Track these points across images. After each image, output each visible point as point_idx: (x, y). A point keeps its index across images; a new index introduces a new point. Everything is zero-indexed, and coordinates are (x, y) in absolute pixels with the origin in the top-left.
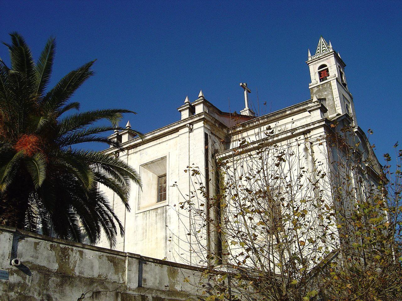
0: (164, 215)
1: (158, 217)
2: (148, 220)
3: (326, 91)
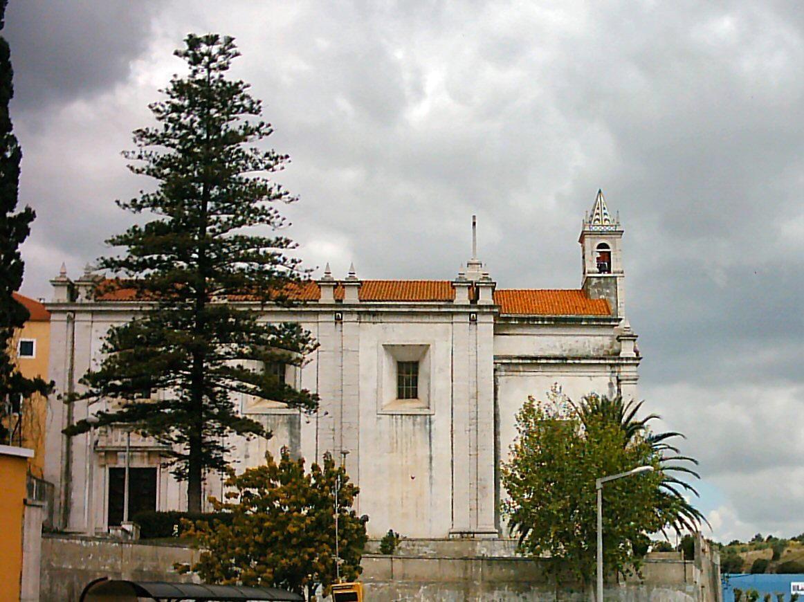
0: (428, 426)
1: (418, 427)
2: (399, 428)
3: (608, 288)
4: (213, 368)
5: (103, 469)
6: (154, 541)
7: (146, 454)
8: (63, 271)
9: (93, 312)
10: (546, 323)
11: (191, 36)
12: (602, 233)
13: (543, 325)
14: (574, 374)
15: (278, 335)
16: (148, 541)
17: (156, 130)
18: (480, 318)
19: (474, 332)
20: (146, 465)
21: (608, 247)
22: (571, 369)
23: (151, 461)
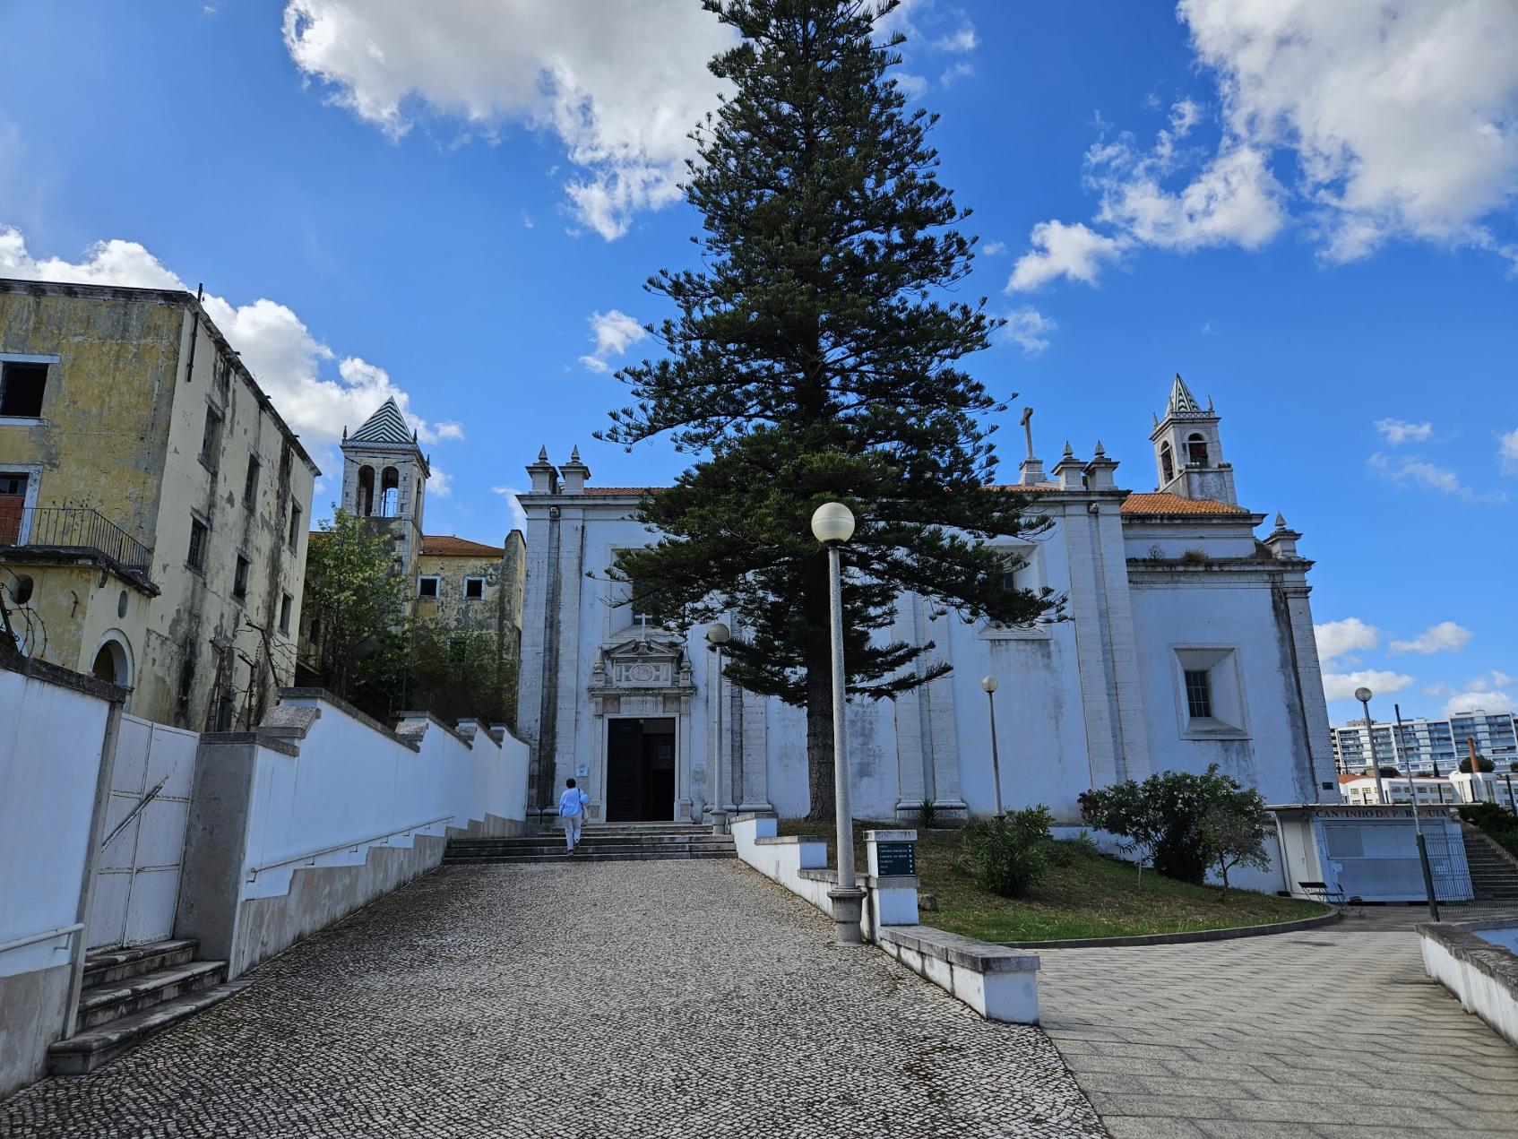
4: (934, 412)
5: (600, 721)
6: (458, 546)
7: (660, 698)
8: (543, 456)
9: (585, 508)
10: (1165, 521)
11: (713, 67)
12: (1193, 421)
13: (1162, 525)
14: (1226, 585)
15: (79, 1097)
16: (465, 546)
17: (645, 363)
18: (1104, 509)
19: (1094, 524)
20: (660, 714)
21: (1200, 439)
22: (1235, 578)
23: (667, 709)
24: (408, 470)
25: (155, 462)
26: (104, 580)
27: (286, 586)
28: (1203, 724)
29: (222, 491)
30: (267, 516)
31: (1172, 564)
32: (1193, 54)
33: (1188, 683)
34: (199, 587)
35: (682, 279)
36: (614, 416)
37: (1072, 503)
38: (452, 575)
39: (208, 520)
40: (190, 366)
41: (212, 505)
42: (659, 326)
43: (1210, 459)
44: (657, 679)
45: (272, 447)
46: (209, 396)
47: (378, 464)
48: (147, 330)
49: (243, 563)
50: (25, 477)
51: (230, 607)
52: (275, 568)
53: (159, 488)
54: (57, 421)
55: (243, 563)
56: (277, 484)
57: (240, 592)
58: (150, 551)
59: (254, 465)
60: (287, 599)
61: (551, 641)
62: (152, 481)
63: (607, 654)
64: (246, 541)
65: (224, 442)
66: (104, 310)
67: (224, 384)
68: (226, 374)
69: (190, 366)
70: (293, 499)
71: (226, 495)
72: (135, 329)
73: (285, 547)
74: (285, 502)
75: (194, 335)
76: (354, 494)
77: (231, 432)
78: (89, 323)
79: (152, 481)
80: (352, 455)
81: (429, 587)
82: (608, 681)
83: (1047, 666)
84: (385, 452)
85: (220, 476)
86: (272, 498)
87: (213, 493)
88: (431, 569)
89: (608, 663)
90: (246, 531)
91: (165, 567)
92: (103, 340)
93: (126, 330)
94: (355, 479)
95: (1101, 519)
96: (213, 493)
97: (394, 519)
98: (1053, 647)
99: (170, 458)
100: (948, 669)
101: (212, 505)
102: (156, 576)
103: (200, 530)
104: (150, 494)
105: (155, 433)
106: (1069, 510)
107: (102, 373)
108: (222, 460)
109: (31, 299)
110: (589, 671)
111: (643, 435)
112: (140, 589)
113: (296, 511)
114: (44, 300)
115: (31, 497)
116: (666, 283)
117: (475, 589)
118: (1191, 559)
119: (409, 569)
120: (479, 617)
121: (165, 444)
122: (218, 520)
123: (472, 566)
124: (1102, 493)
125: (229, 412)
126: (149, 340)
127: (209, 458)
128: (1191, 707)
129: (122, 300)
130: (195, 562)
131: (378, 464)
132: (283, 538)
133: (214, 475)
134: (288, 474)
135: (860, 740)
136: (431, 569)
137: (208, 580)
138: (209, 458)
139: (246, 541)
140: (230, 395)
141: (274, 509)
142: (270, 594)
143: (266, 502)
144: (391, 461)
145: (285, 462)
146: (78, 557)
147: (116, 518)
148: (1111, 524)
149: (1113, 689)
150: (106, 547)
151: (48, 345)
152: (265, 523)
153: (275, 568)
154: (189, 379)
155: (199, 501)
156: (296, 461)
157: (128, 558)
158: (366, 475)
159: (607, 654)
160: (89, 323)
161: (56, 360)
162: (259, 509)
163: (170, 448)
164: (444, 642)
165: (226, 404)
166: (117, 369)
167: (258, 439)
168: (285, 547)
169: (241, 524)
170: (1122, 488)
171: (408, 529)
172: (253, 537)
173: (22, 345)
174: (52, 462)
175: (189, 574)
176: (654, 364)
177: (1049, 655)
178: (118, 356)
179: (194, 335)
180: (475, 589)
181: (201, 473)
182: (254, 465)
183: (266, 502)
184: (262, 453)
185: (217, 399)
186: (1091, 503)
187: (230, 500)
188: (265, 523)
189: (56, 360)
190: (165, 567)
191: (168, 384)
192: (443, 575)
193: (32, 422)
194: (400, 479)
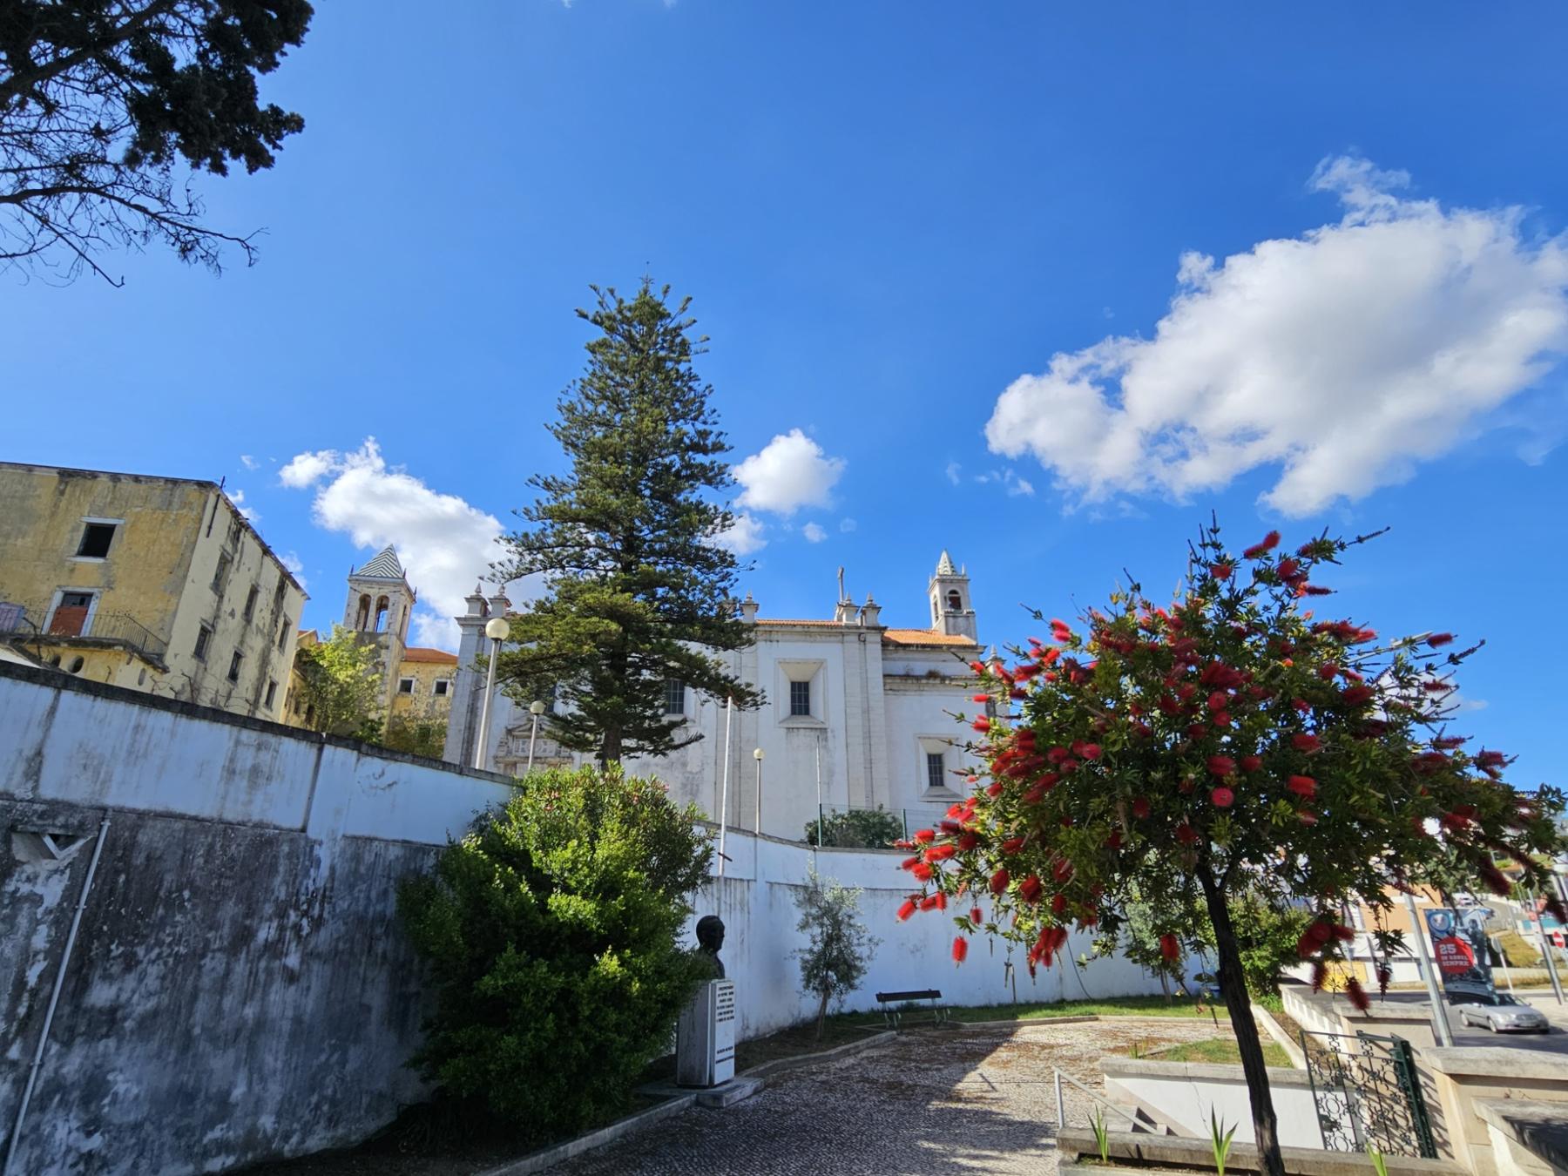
12: (952, 581)
24: (397, 600)
25: (177, 589)
26: (130, 660)
27: (272, 674)
28: (937, 790)
29: (226, 607)
30: (261, 626)
31: (918, 678)
32: (1461, 207)
33: (930, 762)
34: (201, 671)
35: (550, 480)
36: (492, 566)
37: (848, 634)
38: (422, 679)
39: (213, 626)
40: (210, 527)
41: (216, 617)
42: (520, 511)
43: (963, 606)
44: (545, 751)
45: (271, 578)
46: (223, 547)
47: (375, 593)
48: (184, 505)
49: (238, 656)
50: (90, 595)
51: (225, 687)
52: (265, 661)
53: (178, 604)
54: (117, 560)
55: (238, 656)
56: (272, 605)
57: (233, 676)
58: (166, 644)
59: (254, 592)
60: (273, 686)
61: (470, 723)
62: (174, 600)
63: (509, 732)
64: (242, 642)
65: (231, 576)
66: (158, 492)
67: (235, 537)
68: (239, 531)
69: (210, 527)
70: (285, 616)
71: (229, 611)
72: (176, 505)
73: (275, 649)
74: (277, 617)
75: (215, 508)
76: (354, 616)
77: (238, 569)
78: (146, 500)
79: (174, 600)
80: (356, 587)
81: (406, 686)
82: (509, 752)
83: (825, 747)
84: (381, 584)
85: (226, 599)
86: (267, 615)
87: (218, 609)
88: (409, 672)
89: (510, 738)
90: (243, 636)
91: (176, 656)
92: (154, 511)
93: (170, 503)
94: (356, 604)
95: (868, 646)
96: (218, 609)
97: (382, 634)
98: (829, 734)
99: (188, 585)
100: (701, 737)
101: (216, 617)
102: (169, 660)
103: (205, 633)
104: (171, 608)
105: (179, 572)
106: (846, 638)
107: (150, 531)
108: (228, 588)
109: (111, 484)
110: (496, 743)
111: (511, 578)
112: (155, 668)
113: (286, 625)
114: (119, 485)
115: (93, 607)
116: (541, 482)
117: (441, 688)
118: (932, 675)
119: (390, 672)
120: (443, 709)
121: (185, 577)
122: (220, 626)
123: (440, 672)
124: (868, 628)
125: (237, 557)
126: (185, 511)
127: (218, 586)
128: (931, 779)
129: (170, 486)
130: (200, 652)
131: (375, 593)
132: (273, 642)
133: (221, 597)
134: (283, 598)
135: (689, 797)
136: (409, 672)
137: (209, 666)
138: (218, 586)
139: (242, 642)
140: (239, 546)
141: (268, 621)
142: (258, 679)
143: (262, 615)
144: (385, 591)
145: (281, 589)
146: (114, 645)
147: (146, 623)
148: (875, 648)
149: (870, 764)
150: (137, 641)
151: (118, 513)
152: (259, 630)
153: (265, 661)
154: (208, 536)
155: (208, 614)
156: (290, 589)
157: (151, 647)
158: (365, 601)
159: (509, 732)
160: (146, 500)
161: (122, 522)
162: (255, 621)
163: (189, 579)
164: (413, 728)
165: (235, 550)
166: (161, 529)
167: (259, 575)
168: (275, 649)
169: (239, 630)
170: (883, 625)
171: (393, 642)
172: (248, 640)
173: (101, 513)
174: (110, 586)
175: (194, 661)
176: (519, 534)
177: (826, 739)
178: (163, 520)
179: (215, 508)
180: (441, 688)
181: (211, 596)
182: (254, 592)
183: (262, 615)
184: (262, 583)
185: (229, 548)
186: (860, 634)
187: (232, 614)
188: (259, 630)
189: (122, 522)
190: (176, 656)
191: (192, 539)
192: (417, 676)
193: (100, 561)
194: (390, 604)
